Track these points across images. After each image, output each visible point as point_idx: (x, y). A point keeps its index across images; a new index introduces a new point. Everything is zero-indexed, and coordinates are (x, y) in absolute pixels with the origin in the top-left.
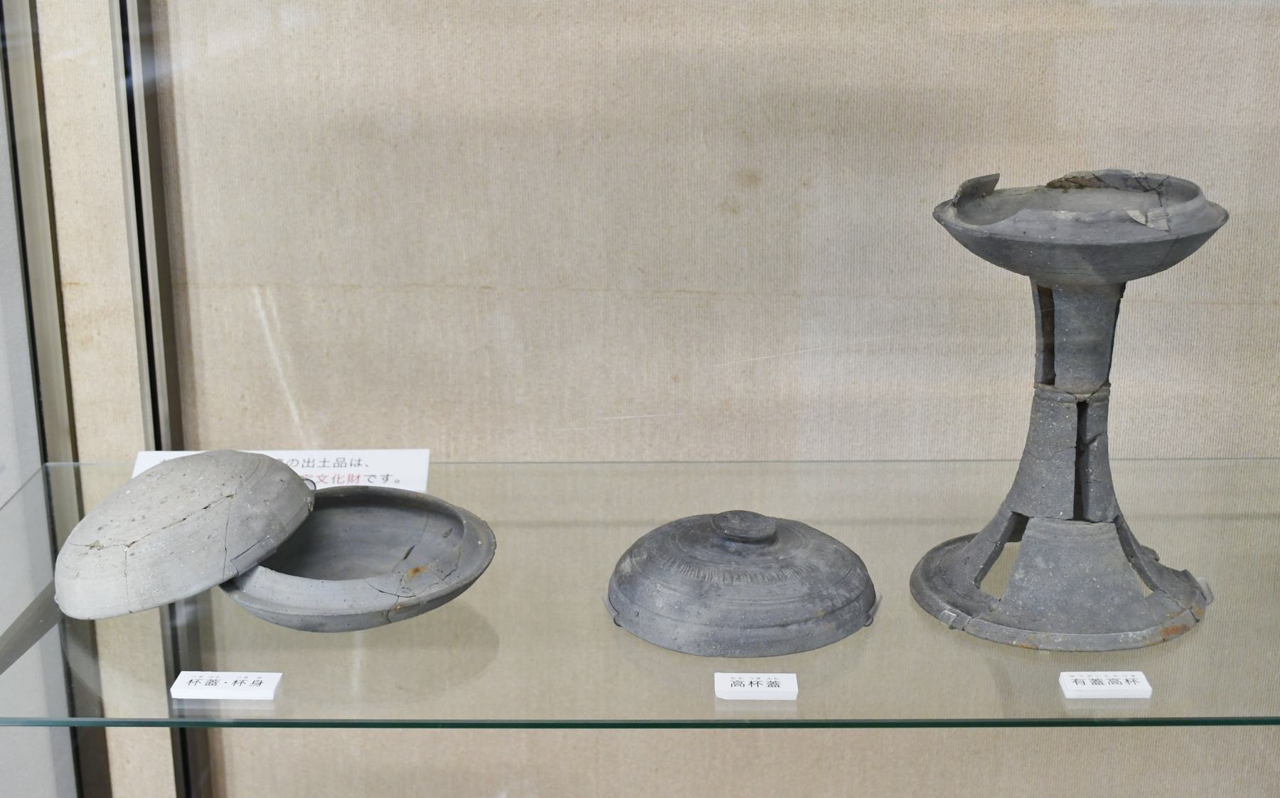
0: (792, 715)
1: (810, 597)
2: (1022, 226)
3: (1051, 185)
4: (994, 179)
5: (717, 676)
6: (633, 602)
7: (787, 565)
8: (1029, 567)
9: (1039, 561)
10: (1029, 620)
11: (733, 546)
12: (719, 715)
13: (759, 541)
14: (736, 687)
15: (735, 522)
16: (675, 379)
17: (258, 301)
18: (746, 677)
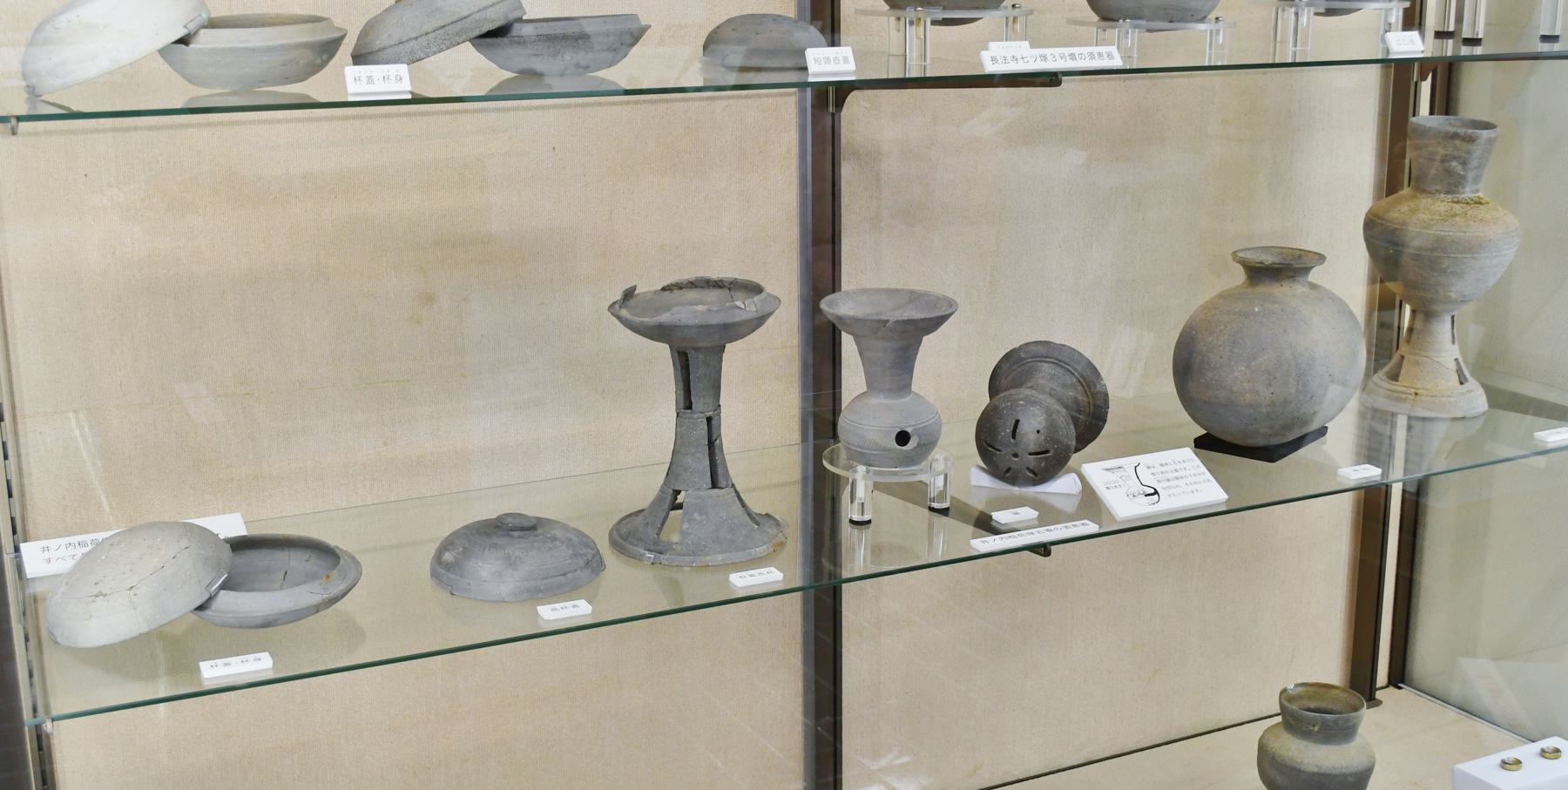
0: (271, 676)
1: (576, 555)
2: (677, 316)
3: (664, 289)
4: (634, 288)
5: (202, 664)
6: (462, 576)
7: (555, 539)
8: (691, 520)
9: (696, 516)
10: (697, 550)
11: (516, 534)
12: (207, 686)
13: (528, 529)
14: (552, 613)
15: (510, 520)
16: (385, 444)
17: (74, 424)
18: (557, 606)
